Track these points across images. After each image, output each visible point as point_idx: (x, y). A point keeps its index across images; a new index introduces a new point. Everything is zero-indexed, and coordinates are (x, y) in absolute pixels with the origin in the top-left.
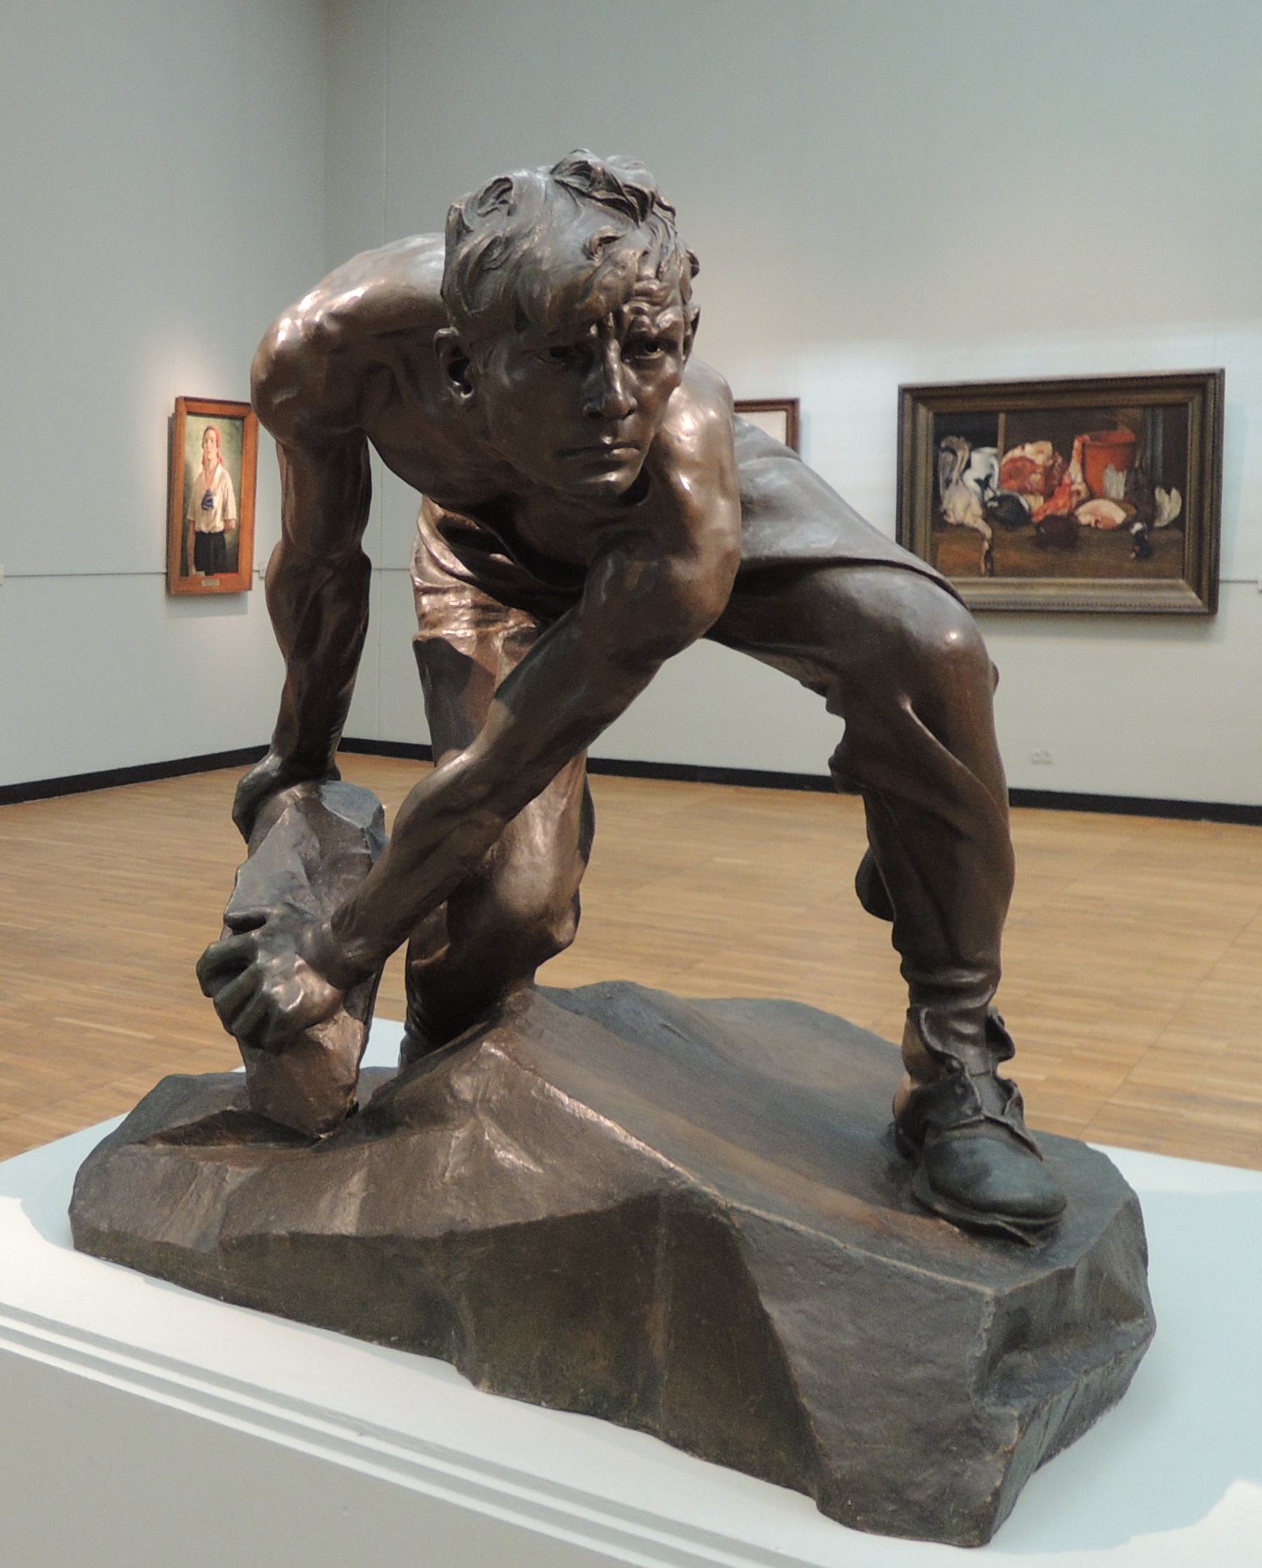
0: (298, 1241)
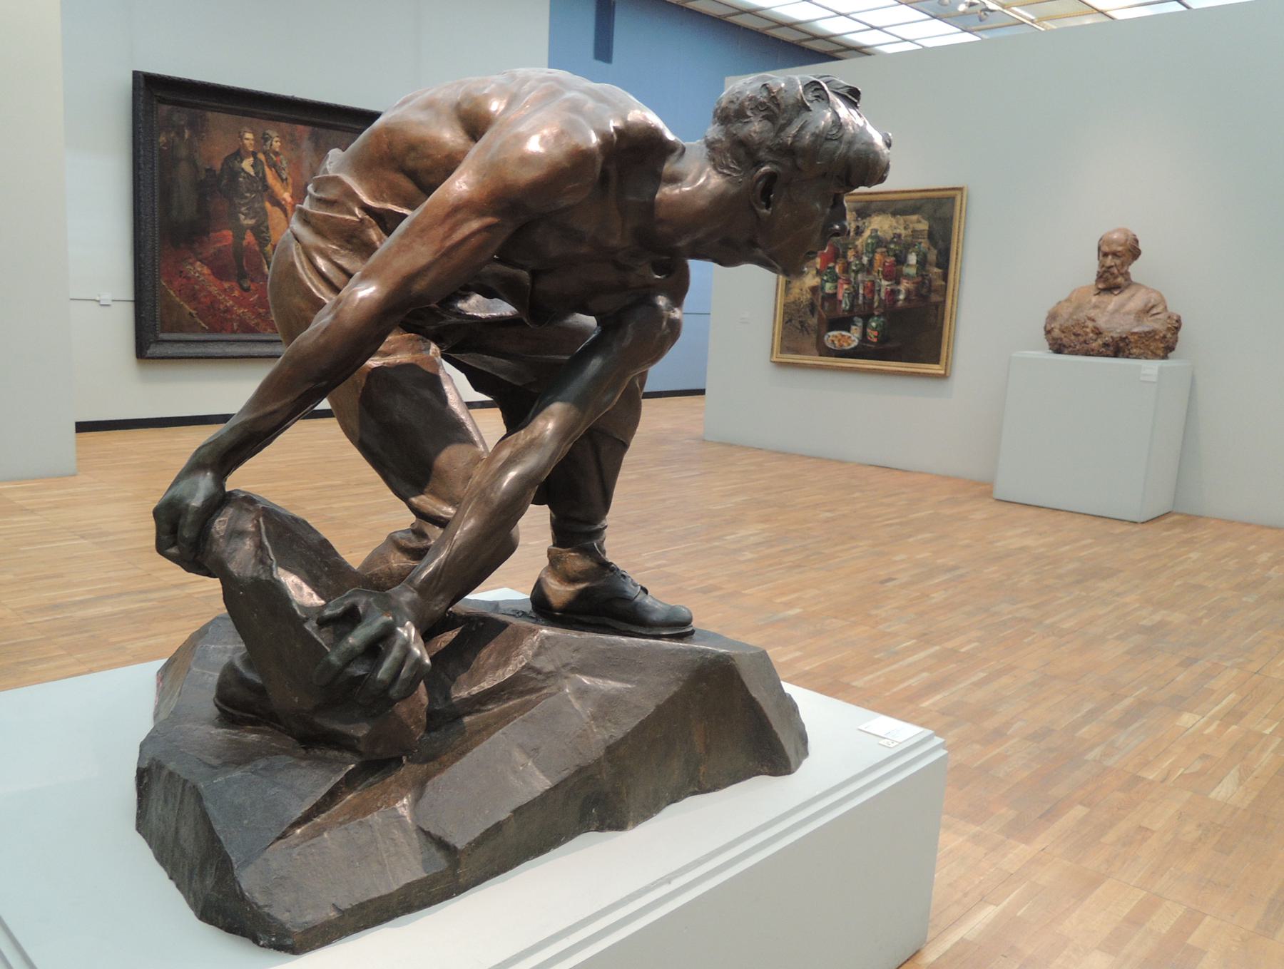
0: (518, 812)
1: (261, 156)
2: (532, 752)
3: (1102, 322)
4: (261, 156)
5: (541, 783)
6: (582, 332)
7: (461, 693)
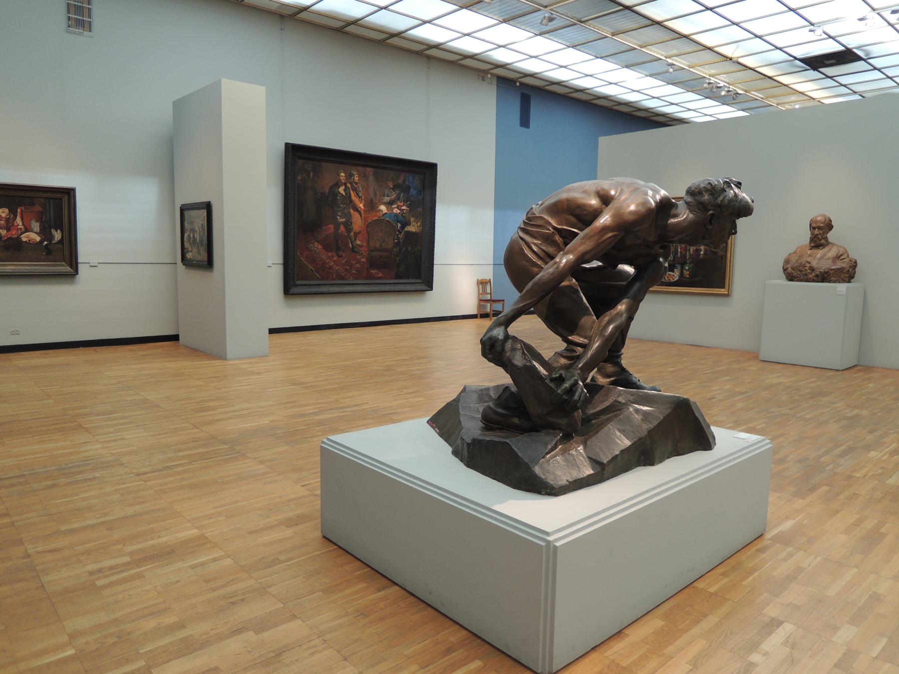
0: (622, 452)
1: (349, 185)
2: (623, 431)
3: (814, 264)
4: (349, 185)
5: (627, 443)
6: (625, 274)
7: (591, 411)
